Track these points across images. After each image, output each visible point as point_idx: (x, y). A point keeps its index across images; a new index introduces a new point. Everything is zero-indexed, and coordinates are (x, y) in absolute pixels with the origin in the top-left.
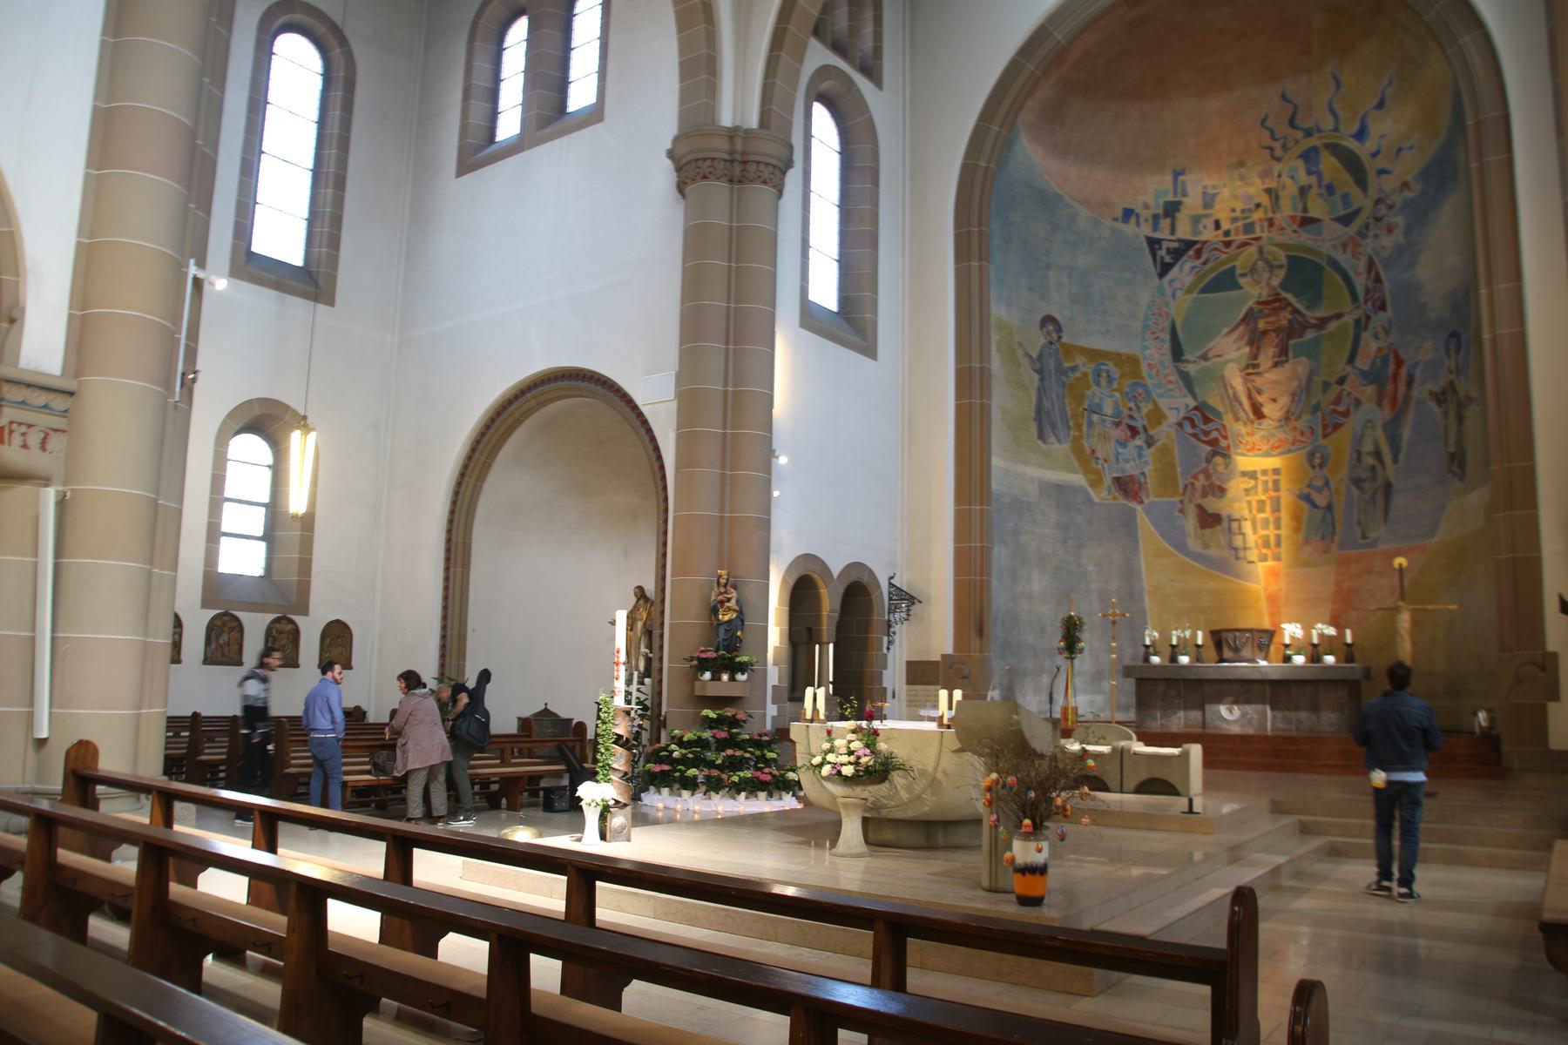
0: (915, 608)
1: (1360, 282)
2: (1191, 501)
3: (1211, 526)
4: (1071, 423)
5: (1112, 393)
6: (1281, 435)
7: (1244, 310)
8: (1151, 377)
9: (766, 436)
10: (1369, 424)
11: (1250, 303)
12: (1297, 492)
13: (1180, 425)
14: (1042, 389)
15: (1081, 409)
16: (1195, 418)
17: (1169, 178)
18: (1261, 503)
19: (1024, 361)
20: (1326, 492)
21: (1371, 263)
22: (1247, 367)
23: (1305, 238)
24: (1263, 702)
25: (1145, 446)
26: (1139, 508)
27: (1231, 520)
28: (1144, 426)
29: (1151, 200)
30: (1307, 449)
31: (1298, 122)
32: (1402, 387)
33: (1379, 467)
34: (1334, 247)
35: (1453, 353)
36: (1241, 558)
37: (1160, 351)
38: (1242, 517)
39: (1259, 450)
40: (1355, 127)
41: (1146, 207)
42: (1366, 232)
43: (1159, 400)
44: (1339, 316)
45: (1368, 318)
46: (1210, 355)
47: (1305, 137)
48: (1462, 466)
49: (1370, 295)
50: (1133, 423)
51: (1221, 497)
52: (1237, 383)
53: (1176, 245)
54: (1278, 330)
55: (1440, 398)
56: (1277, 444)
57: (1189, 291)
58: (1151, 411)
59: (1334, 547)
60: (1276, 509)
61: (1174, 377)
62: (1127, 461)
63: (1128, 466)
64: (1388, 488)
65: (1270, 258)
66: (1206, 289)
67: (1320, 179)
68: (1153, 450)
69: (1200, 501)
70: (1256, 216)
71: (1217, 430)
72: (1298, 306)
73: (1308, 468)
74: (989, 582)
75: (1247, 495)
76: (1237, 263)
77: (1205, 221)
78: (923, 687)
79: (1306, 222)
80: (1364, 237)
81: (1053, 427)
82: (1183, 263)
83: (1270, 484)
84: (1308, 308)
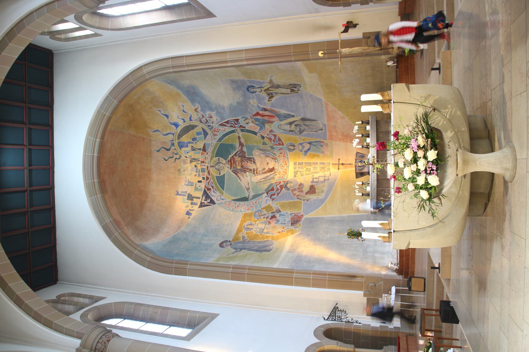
1: (228, 129)
3: (315, 189)
4: (266, 240)
5: (256, 224)
8: (253, 209)
9: (110, 96)
10: (279, 127)
11: (231, 171)
13: (273, 199)
16: (271, 194)
17: (179, 197)
19: (235, 254)
20: (304, 145)
21: (221, 125)
23: (210, 150)
24: (386, 154)
25: (280, 213)
26: (305, 217)
27: (313, 182)
28: (272, 213)
30: (287, 151)
31: (168, 148)
32: (266, 113)
33: (295, 123)
34: (214, 139)
35: (254, 90)
36: (329, 178)
40: (174, 127)
41: (187, 206)
44: (239, 138)
45: (241, 126)
46: (247, 187)
47: (174, 146)
48: (295, 86)
50: (270, 217)
51: (303, 185)
52: (259, 177)
53: (204, 197)
55: (271, 96)
56: (285, 163)
57: (222, 194)
58: (266, 210)
60: (310, 164)
61: (254, 201)
62: (285, 220)
63: (287, 220)
64: (303, 119)
67: (190, 143)
68: (281, 210)
69: (304, 193)
70: (199, 167)
71: (276, 186)
72: (234, 153)
73: (294, 151)
74: (329, 272)
76: (215, 175)
79: (204, 149)
80: (212, 127)
83: (300, 166)
84: (235, 150)
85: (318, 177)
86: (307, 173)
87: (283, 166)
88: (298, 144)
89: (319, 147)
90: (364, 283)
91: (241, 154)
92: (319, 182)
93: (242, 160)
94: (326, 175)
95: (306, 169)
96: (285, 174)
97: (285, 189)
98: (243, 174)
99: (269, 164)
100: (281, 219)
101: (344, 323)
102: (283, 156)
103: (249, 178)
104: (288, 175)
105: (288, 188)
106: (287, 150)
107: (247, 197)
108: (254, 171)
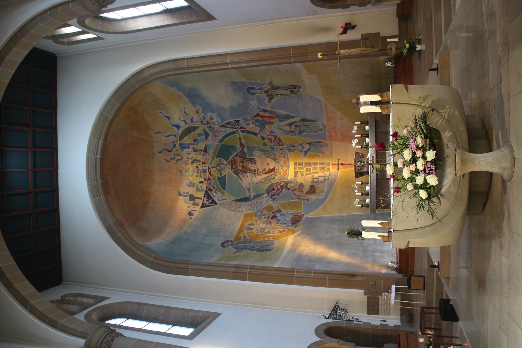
0: (341, 306)
1: (229, 130)
2: (304, 197)
3: (315, 189)
5: (257, 224)
6: (282, 162)
7: (234, 174)
8: (254, 209)
11: (232, 172)
12: (304, 156)
13: (274, 200)
14: (250, 249)
15: (262, 235)
16: (272, 194)
17: (180, 197)
18: (307, 170)
19: (237, 254)
20: (304, 145)
21: (222, 126)
22: (255, 174)
23: (211, 151)
25: (280, 213)
26: (305, 216)
27: (313, 182)
28: (272, 213)
29: (186, 206)
30: (288, 152)
32: (267, 114)
34: (215, 140)
35: (255, 91)
36: (328, 178)
37: (244, 205)
38: (312, 177)
39: (286, 170)
41: (189, 207)
42: (212, 128)
43: (263, 207)
44: (240, 139)
45: (242, 127)
46: (248, 187)
47: (176, 147)
49: (234, 127)
50: (271, 217)
51: (304, 185)
52: (260, 178)
53: (206, 198)
54: (243, 162)
55: (271, 97)
56: (285, 163)
57: (223, 194)
58: (267, 210)
59: (325, 142)
60: (310, 164)
61: (255, 201)
62: (285, 220)
63: (288, 220)
64: (303, 120)
65: (216, 164)
66: (224, 188)
67: (191, 144)
68: (282, 210)
69: (305, 193)
70: (201, 168)
71: (277, 186)
75: (304, 175)
76: (216, 176)
77: (199, 187)
78: (380, 306)
79: (205, 150)
80: (213, 128)
81: (267, 246)
82: (212, 195)
83: (300, 166)
84: (236, 151)
85: (318, 177)
86: (307, 173)
87: (283, 166)
88: (298, 144)
89: (319, 147)
90: (365, 281)
91: (242, 155)
92: (318, 182)
93: (243, 161)
94: (326, 175)
95: (306, 169)
96: (285, 174)
97: (286, 189)
98: (244, 175)
99: (270, 165)
100: (281, 218)
101: (345, 322)
102: (283, 157)
103: (250, 178)
104: (288, 175)
105: (289, 188)
106: (287, 151)
107: (248, 197)
108: (255, 171)
